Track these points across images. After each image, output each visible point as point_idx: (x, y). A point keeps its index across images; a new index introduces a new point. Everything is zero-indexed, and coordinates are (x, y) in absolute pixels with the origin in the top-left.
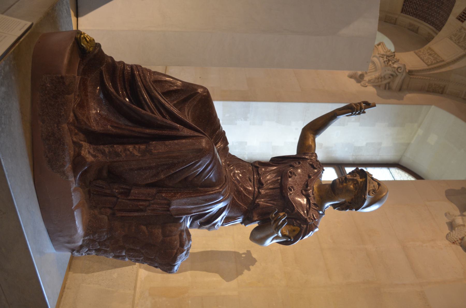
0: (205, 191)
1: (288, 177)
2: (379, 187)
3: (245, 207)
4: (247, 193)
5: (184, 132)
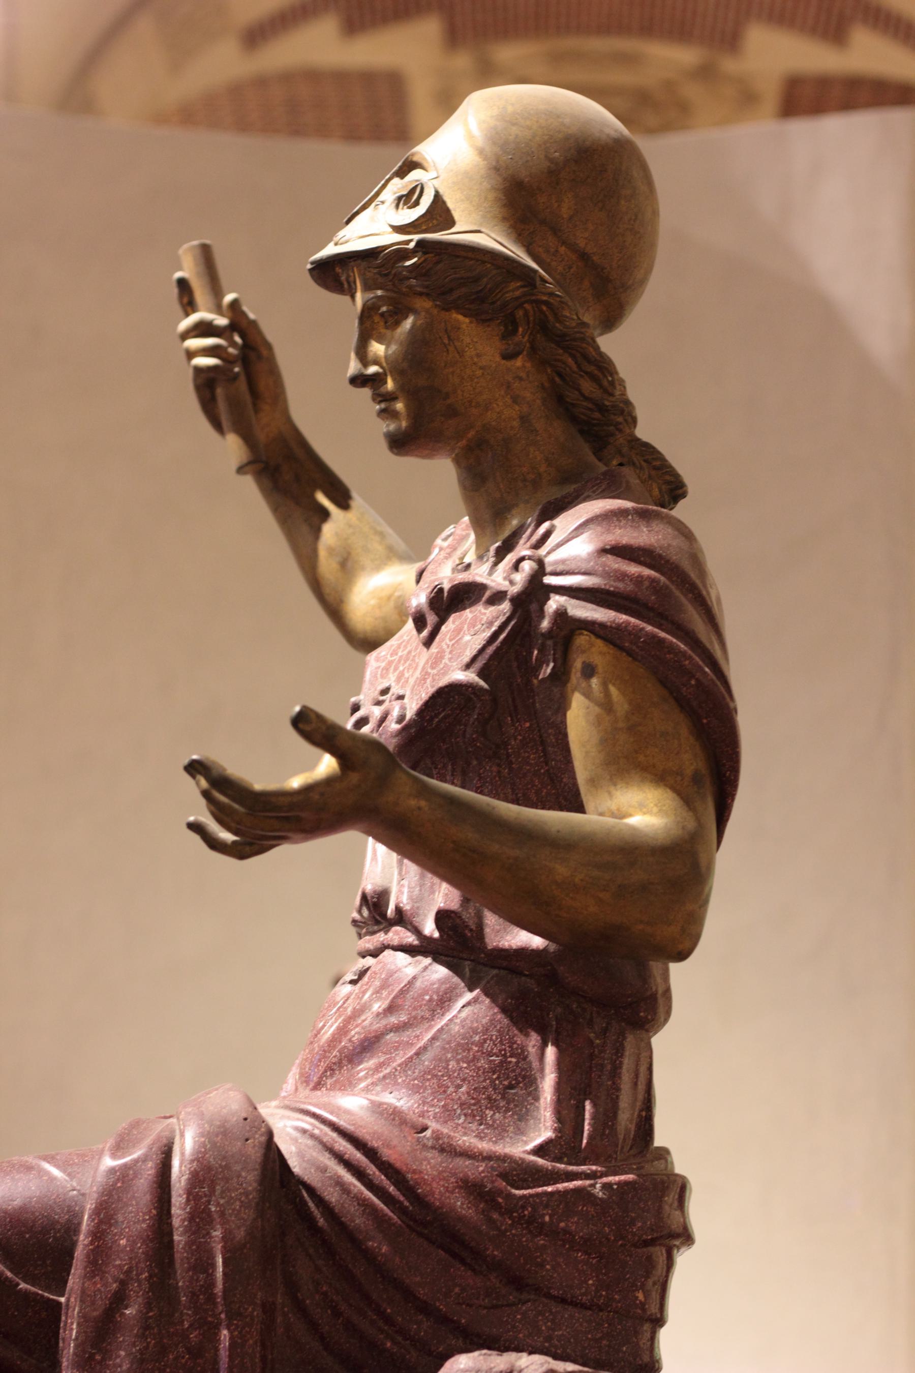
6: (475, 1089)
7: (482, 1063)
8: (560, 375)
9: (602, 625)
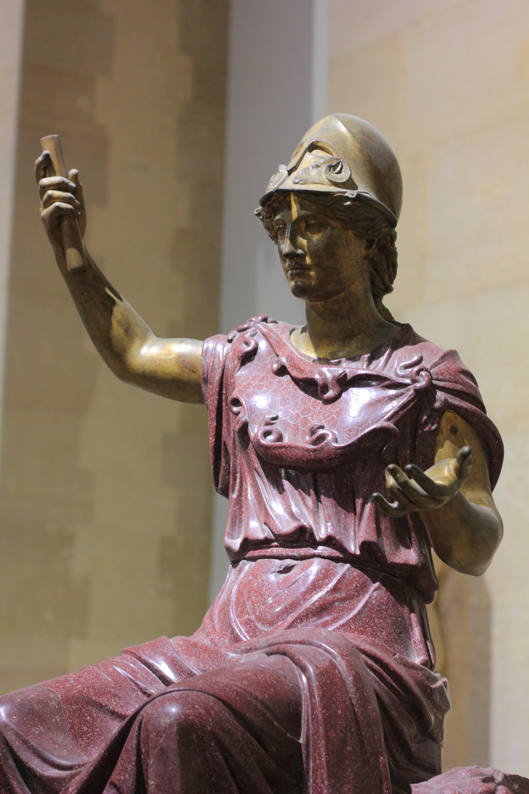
0: (313, 720)
1: (279, 443)
2: (322, 149)
3: (372, 589)
4: (327, 581)
5: (124, 781)
6: (389, 633)
7: (388, 620)
8: (375, 270)
9: (466, 410)
